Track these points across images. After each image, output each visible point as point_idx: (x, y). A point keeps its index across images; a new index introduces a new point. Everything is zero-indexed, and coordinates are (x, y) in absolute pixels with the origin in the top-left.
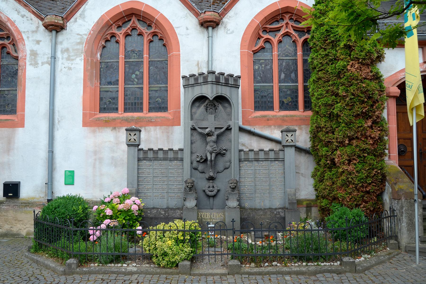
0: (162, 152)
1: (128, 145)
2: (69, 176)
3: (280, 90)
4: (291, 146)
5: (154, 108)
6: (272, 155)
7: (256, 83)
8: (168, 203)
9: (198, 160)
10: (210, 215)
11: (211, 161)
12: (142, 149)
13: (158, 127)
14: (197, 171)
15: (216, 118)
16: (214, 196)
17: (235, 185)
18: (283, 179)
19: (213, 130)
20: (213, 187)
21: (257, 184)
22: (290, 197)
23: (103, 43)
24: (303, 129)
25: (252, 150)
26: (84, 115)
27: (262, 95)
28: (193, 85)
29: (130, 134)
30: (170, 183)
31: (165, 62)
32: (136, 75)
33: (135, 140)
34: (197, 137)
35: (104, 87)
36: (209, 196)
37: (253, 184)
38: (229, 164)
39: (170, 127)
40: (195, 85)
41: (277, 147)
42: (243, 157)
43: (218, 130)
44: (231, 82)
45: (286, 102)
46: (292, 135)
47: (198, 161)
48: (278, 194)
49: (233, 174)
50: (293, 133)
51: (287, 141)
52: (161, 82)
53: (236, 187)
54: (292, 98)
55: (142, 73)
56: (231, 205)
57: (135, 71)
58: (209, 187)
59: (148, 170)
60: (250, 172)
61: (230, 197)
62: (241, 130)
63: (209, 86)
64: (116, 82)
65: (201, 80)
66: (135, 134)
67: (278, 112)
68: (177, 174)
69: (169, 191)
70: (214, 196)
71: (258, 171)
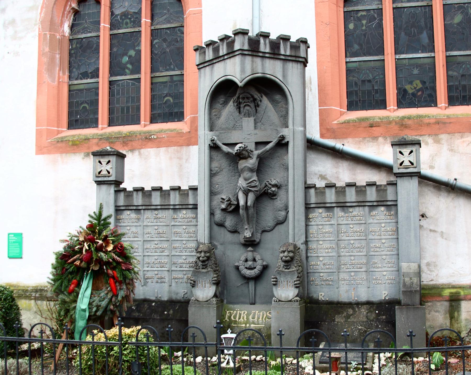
0: (158, 193)
1: (99, 183)
2: (14, 242)
3: (399, 67)
4: (411, 175)
5: (159, 115)
6: (372, 195)
7: (351, 57)
8: (170, 292)
9: (223, 206)
10: (248, 315)
11: (246, 207)
12: (125, 190)
13: (163, 149)
14: (222, 229)
15: (259, 124)
16: (257, 279)
17: (291, 254)
18: (394, 243)
19: (251, 146)
20: (254, 260)
21: (342, 254)
22: (407, 279)
23: (74, 5)
24: (443, 142)
25: (330, 186)
26: (39, 133)
27: (363, 79)
28: (211, 63)
29: (100, 162)
30: (174, 253)
31: (179, 30)
32: (130, 57)
33: (109, 172)
34: (221, 163)
35: (76, 82)
36: (247, 279)
37: (334, 254)
38: (283, 213)
39: (185, 148)
40: (214, 61)
41: (380, 178)
42: (313, 199)
43: (262, 146)
44: (285, 51)
45: (410, 91)
46: (411, 152)
47: (223, 210)
48: (385, 273)
49: (294, 232)
50: (414, 148)
51: (401, 164)
52: (172, 67)
53: (292, 258)
54: (423, 83)
55: (139, 52)
56: (283, 295)
57: (128, 50)
58: (246, 261)
59: (134, 229)
60: (327, 229)
61: (281, 279)
62: (312, 145)
63: (238, 59)
64: (95, 74)
65: (223, 50)
66: (109, 162)
67: (395, 110)
68: (187, 235)
69: (173, 269)
70: (257, 279)
71: (343, 227)
